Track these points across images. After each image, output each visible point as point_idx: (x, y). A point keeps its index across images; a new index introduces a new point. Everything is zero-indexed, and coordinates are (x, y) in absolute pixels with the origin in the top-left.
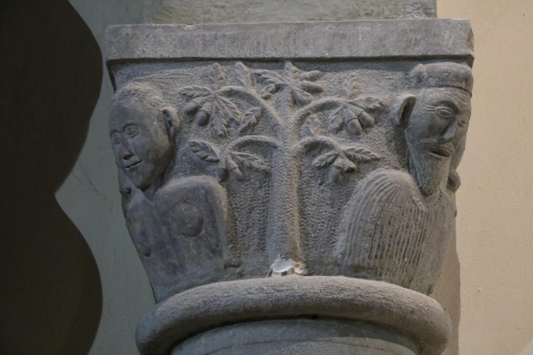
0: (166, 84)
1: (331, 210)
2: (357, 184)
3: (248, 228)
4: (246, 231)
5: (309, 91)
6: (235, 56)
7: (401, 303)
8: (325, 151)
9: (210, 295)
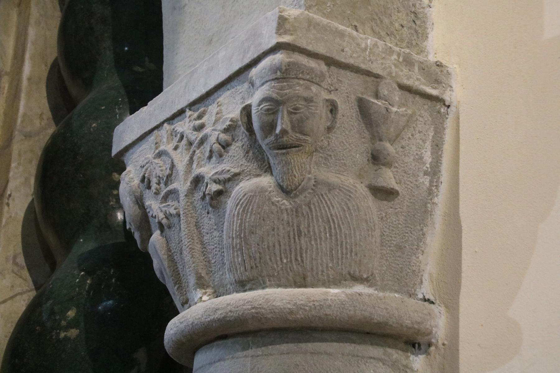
7: (274, 308)
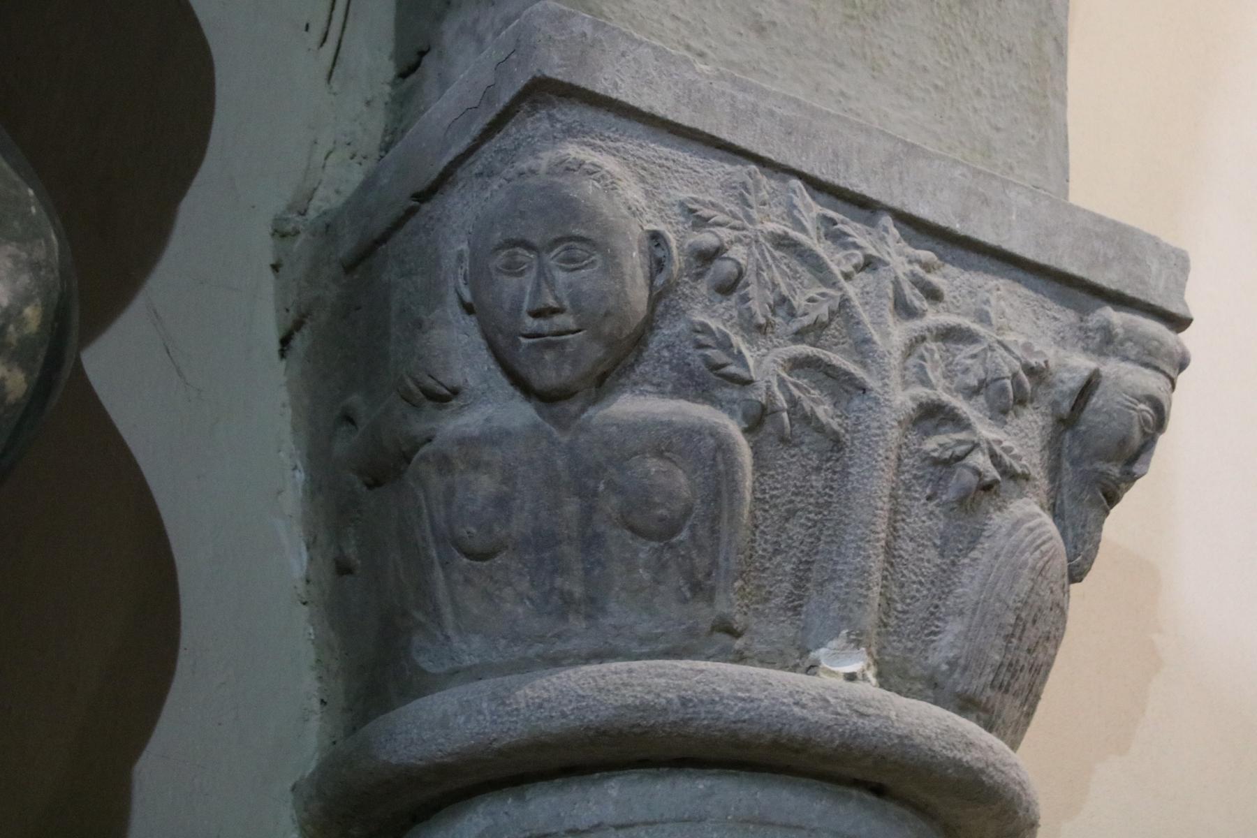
0: (652, 174)
1: (939, 561)
2: (990, 519)
3: (776, 552)
4: (770, 559)
5: (922, 290)
6: (793, 163)
8: (947, 428)
9: (700, 688)
